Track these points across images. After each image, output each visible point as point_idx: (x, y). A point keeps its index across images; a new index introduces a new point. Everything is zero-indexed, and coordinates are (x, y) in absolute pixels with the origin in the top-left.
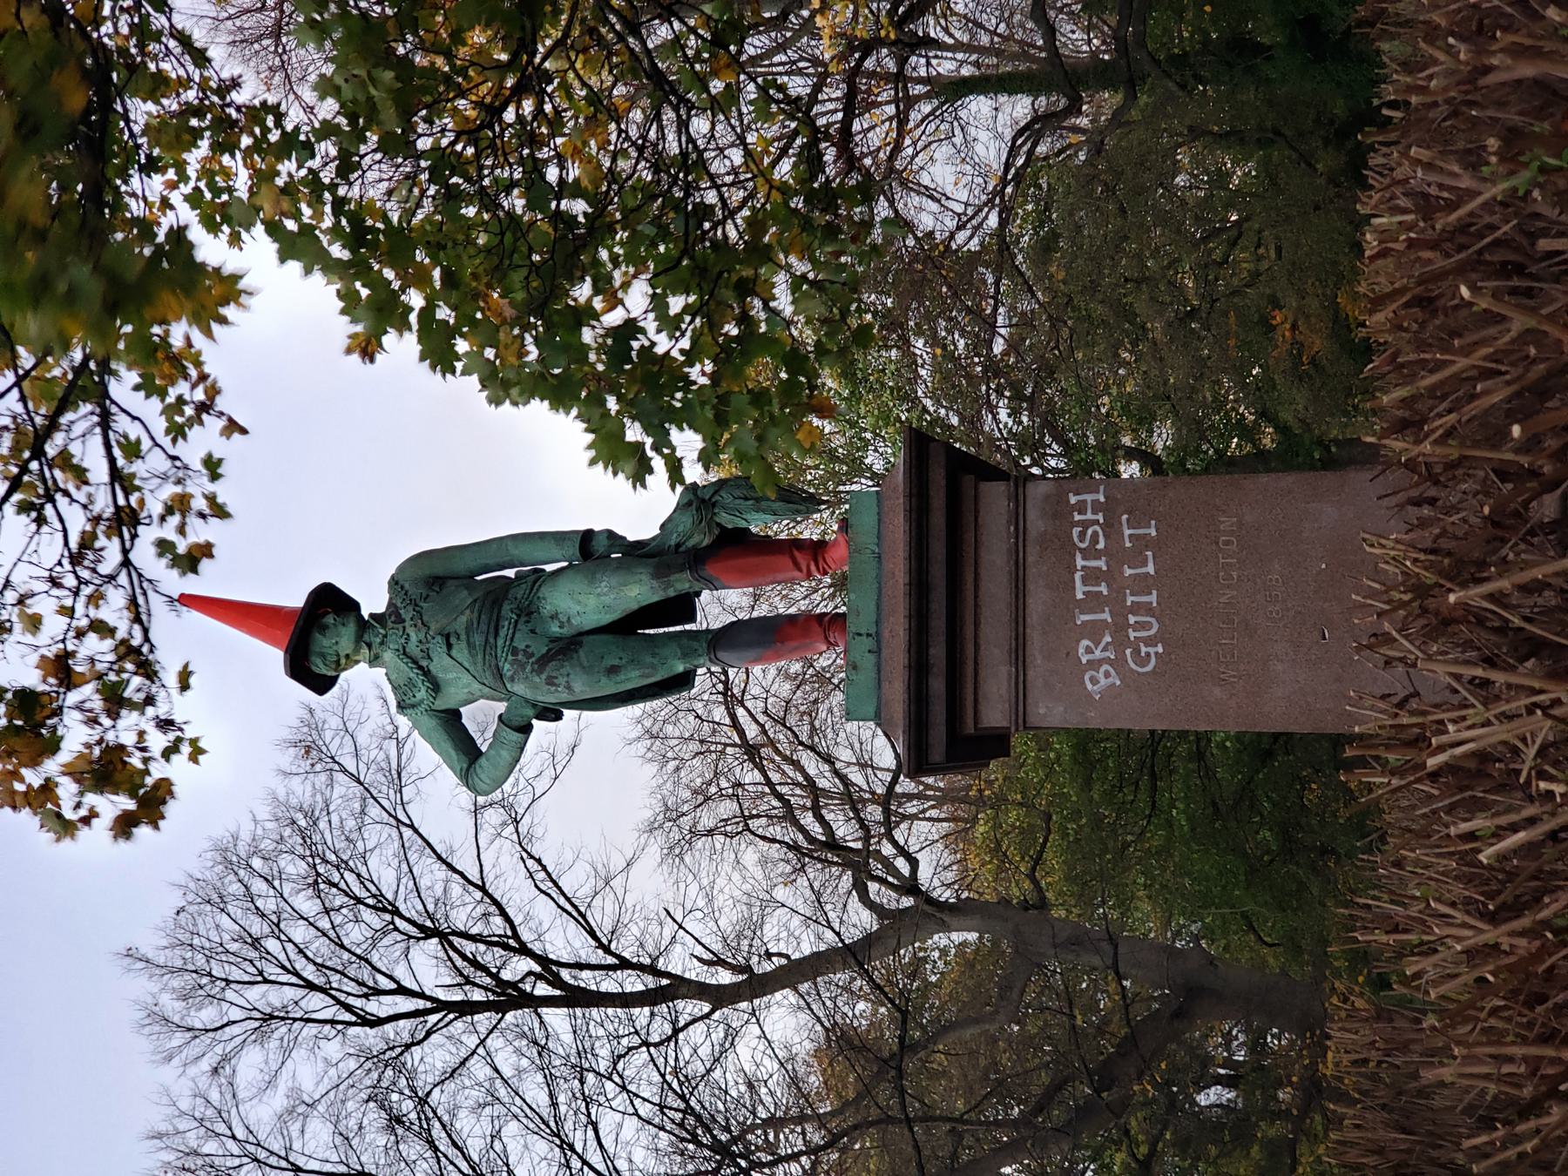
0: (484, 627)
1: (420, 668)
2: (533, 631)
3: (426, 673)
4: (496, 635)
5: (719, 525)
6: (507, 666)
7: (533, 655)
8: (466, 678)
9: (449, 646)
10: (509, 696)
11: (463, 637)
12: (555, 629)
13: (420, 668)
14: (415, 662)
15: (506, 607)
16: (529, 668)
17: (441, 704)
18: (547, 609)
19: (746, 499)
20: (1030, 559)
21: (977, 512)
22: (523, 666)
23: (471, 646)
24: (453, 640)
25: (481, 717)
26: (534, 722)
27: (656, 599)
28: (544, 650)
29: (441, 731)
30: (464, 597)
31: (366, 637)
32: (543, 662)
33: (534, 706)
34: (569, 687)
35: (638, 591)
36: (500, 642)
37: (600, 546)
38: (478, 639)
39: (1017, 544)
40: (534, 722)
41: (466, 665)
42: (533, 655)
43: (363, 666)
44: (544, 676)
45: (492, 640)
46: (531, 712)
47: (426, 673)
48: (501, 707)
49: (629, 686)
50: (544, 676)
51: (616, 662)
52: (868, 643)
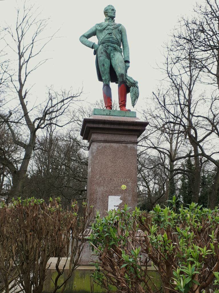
0: (113, 40)
1: (105, 28)
2: (112, 50)
3: (104, 29)
4: (111, 43)
5: (131, 87)
6: (105, 45)
7: (107, 50)
8: (103, 37)
9: (109, 34)
10: (99, 45)
11: (111, 37)
12: (112, 54)
13: (105, 28)
14: (106, 27)
15: (116, 45)
16: (104, 49)
17: (97, 32)
18: (116, 53)
19: (135, 92)
20: (123, 144)
21: (120, 134)
22: (105, 48)
23: (109, 38)
24: (110, 34)
25: (94, 40)
26: (94, 49)
27: (117, 74)
28: (108, 52)
29: (92, 31)
30: (119, 37)
31: (111, 19)
32: (106, 52)
33: (97, 50)
34: (101, 56)
35: (119, 70)
36: (110, 44)
37: (127, 64)
38: (111, 39)
39: (126, 142)
40: (94, 49)
41: (105, 37)
42: (107, 50)
43: (105, 18)
44: (103, 52)
45: (110, 42)
46: (96, 49)
47: (104, 29)
48: (97, 43)
49: (100, 68)
50: (103, 52)
51: (105, 66)
52: (108, 114)
